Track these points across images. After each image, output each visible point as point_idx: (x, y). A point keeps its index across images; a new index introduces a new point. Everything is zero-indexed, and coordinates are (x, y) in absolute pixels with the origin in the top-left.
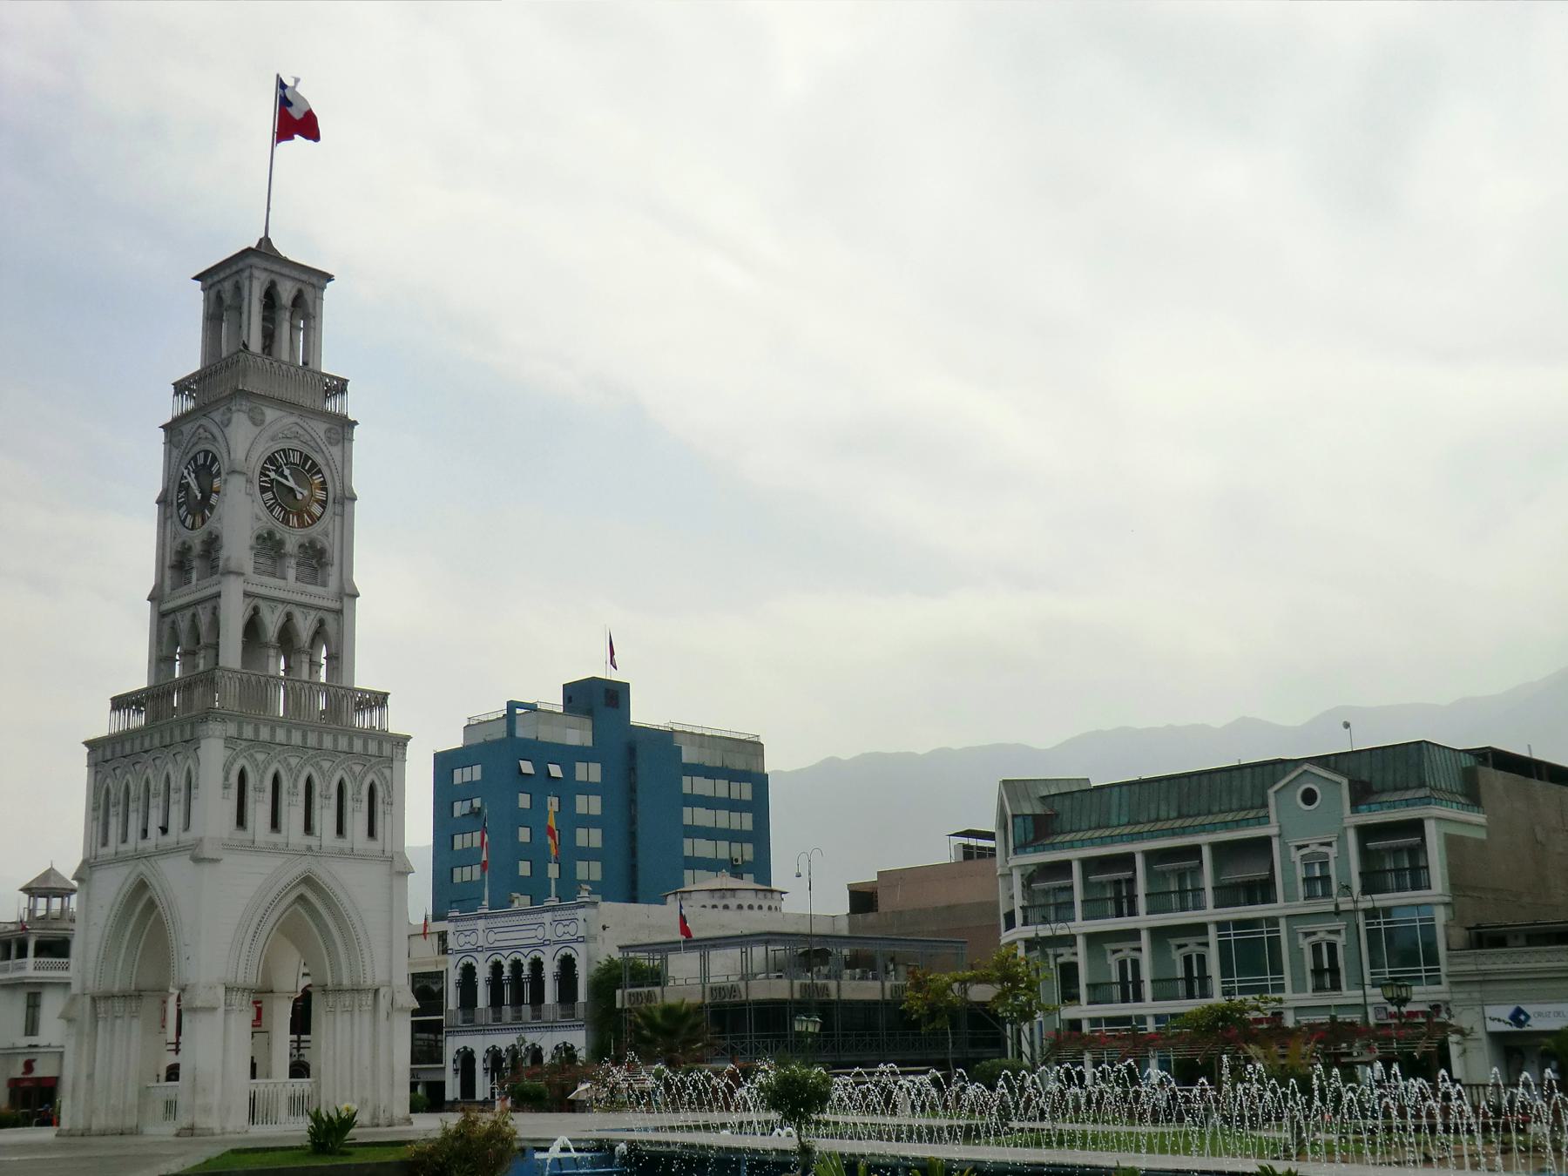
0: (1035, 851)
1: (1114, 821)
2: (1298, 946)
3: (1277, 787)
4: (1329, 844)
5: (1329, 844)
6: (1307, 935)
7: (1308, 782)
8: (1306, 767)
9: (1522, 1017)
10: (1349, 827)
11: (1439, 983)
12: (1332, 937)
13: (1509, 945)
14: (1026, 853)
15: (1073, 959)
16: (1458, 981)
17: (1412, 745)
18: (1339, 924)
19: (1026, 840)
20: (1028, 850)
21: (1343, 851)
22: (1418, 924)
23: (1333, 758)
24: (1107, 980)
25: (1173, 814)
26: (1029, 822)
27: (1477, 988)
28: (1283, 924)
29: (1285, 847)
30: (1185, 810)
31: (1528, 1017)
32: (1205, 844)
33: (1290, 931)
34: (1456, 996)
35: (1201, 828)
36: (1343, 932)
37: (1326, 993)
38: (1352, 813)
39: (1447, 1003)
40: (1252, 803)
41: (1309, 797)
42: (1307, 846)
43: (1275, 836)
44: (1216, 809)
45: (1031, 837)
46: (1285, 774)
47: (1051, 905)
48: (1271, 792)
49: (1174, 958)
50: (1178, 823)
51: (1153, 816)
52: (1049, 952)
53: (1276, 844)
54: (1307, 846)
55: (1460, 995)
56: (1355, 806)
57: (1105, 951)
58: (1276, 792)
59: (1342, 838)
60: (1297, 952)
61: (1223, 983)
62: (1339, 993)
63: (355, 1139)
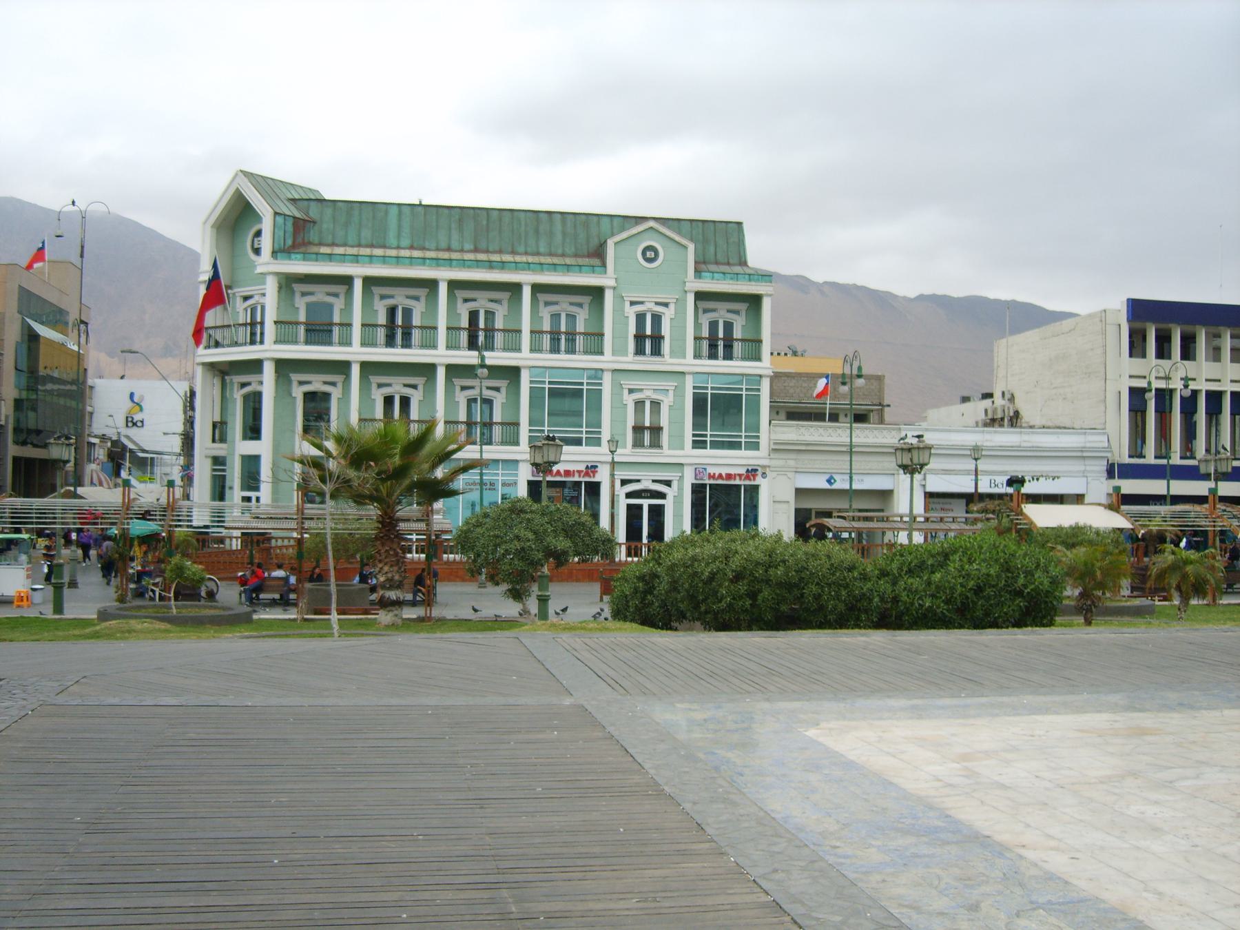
0: (304, 259)
1: (393, 241)
2: (622, 401)
3: (618, 238)
4: (666, 305)
5: (666, 305)
6: (631, 391)
7: (653, 240)
8: (652, 224)
9: (833, 481)
10: (690, 291)
11: (599, 445)
12: (408, 391)
13: (840, 420)
14: (290, 259)
15: (258, 388)
16: (779, 449)
17: (340, 204)
18: (670, 384)
19: (284, 244)
20: (293, 256)
21: (681, 311)
22: (547, 386)
23: (606, 220)
24: (371, 417)
25: (468, 246)
26: (290, 223)
27: (793, 456)
28: (607, 379)
29: (619, 299)
30: (483, 245)
31: (835, 481)
32: (358, 277)
33: (616, 388)
34: (773, 463)
35: (526, 266)
36: (671, 393)
37: (645, 450)
38: (695, 278)
39: (764, 467)
40: (564, 250)
41: (650, 254)
42: (642, 303)
43: (610, 287)
44: (521, 249)
45: (289, 242)
46: (623, 229)
47: (301, 323)
48: (610, 243)
49: (235, 396)
50: (470, 256)
51: (444, 245)
52: (293, 378)
53: (609, 296)
54: (642, 303)
55: (778, 461)
56: (698, 272)
57: (370, 383)
58: (615, 244)
59: (680, 303)
60: (618, 406)
61: (758, 437)
62: (660, 451)
63: (232, 609)
